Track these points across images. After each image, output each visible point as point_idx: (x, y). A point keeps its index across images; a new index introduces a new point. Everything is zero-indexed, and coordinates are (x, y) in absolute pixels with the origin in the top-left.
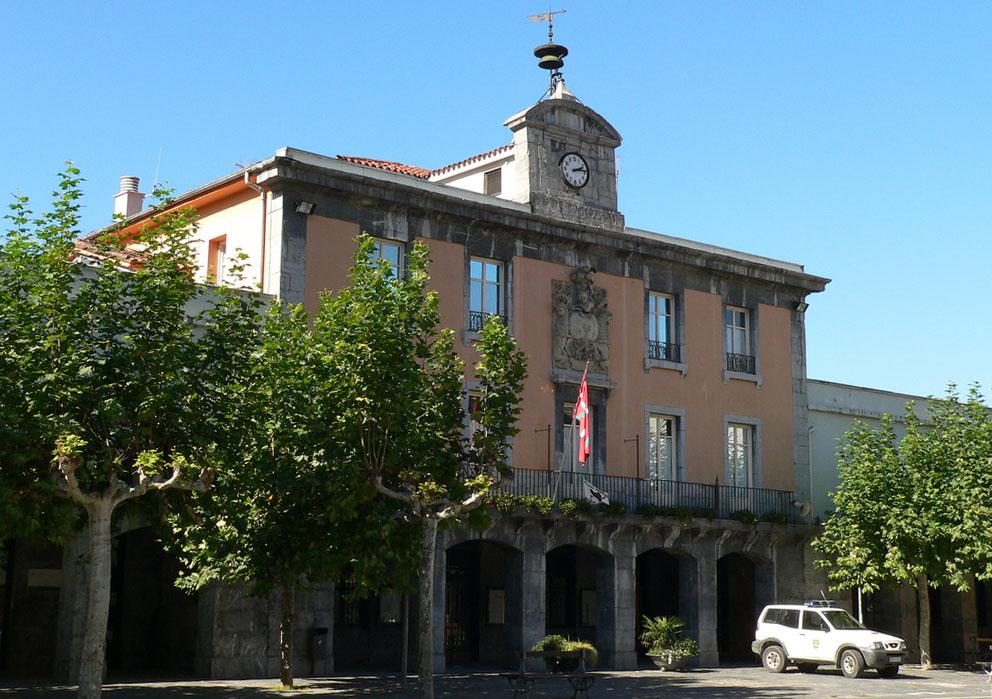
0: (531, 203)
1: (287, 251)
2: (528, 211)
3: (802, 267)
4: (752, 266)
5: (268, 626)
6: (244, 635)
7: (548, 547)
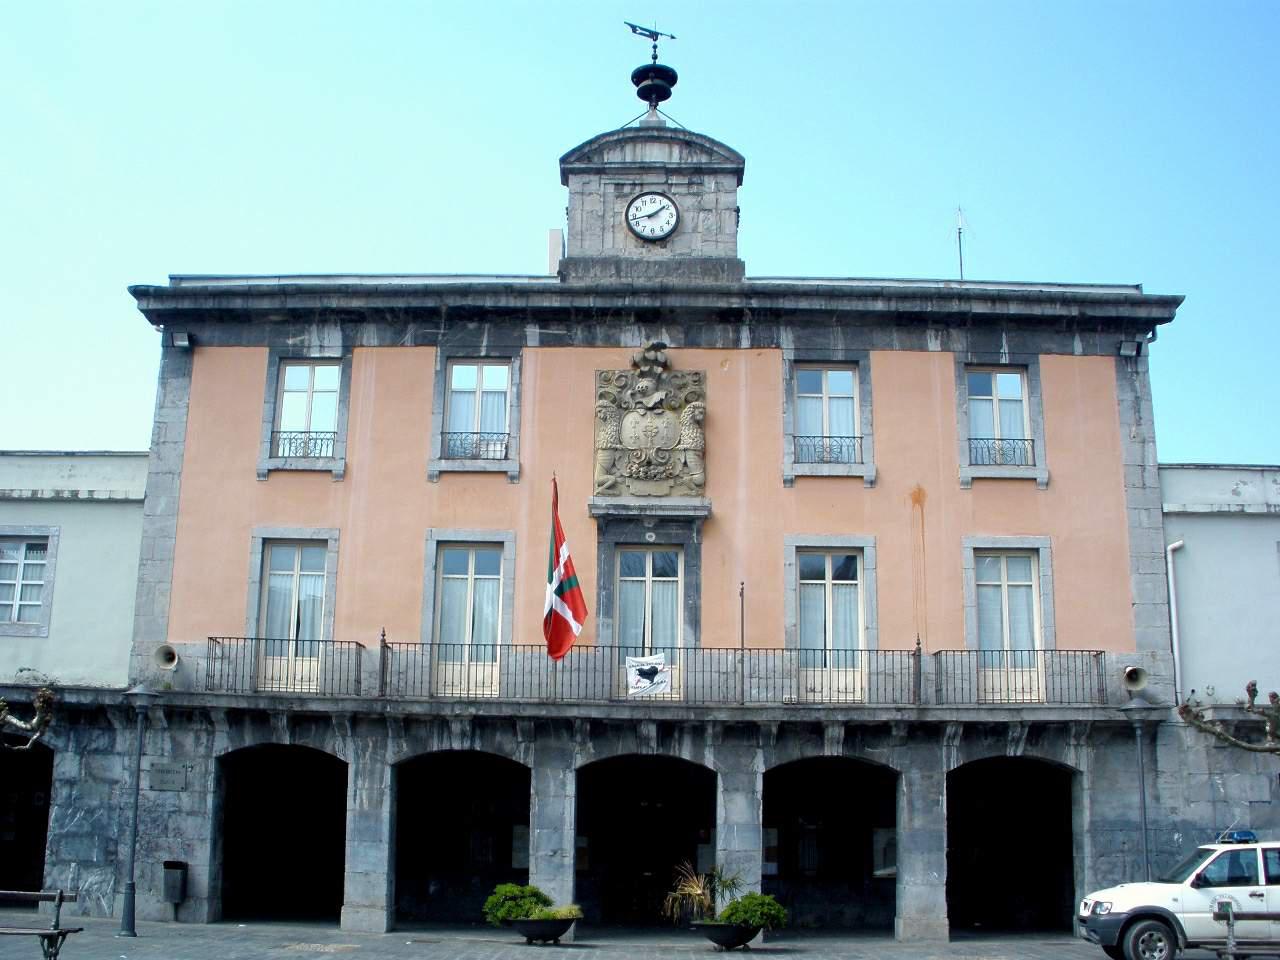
0: (562, 274)
1: (165, 396)
2: (557, 281)
3: (1137, 287)
4: (283, 292)
5: (117, 855)
6: (86, 864)
7: (580, 761)
